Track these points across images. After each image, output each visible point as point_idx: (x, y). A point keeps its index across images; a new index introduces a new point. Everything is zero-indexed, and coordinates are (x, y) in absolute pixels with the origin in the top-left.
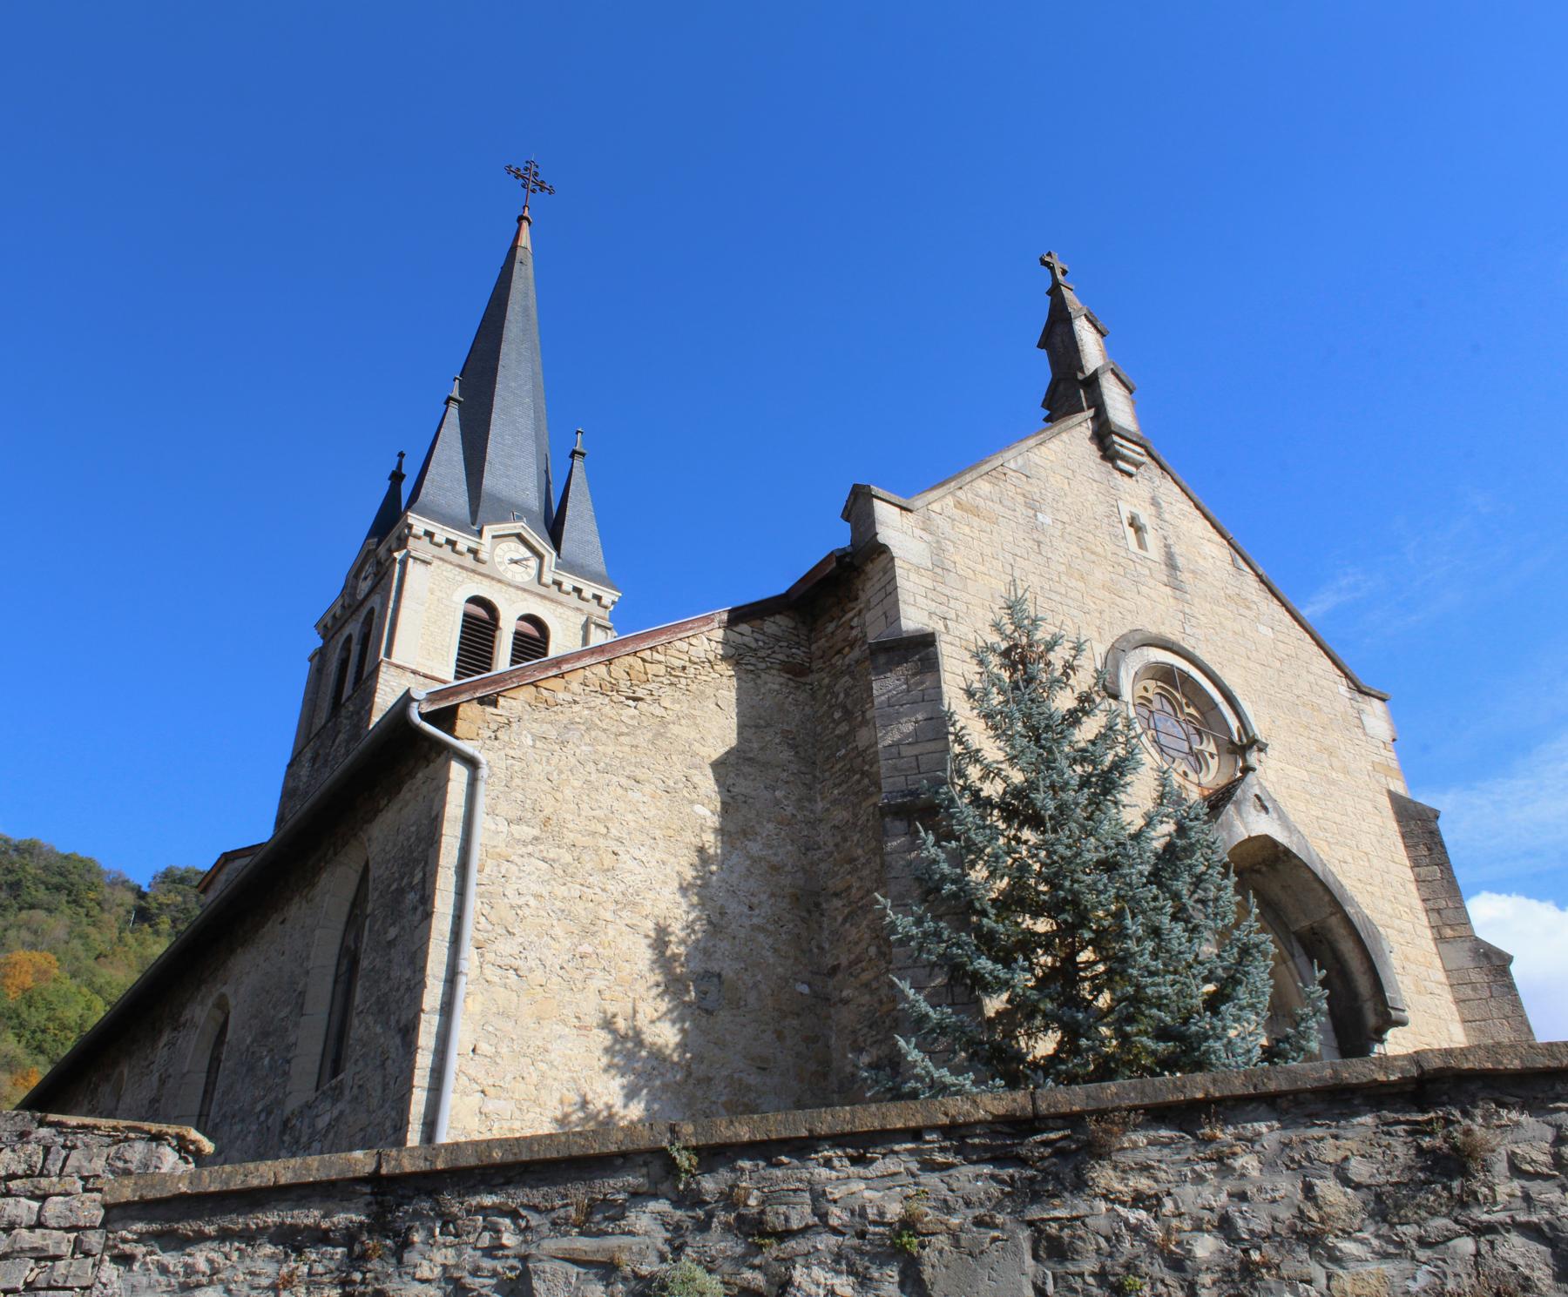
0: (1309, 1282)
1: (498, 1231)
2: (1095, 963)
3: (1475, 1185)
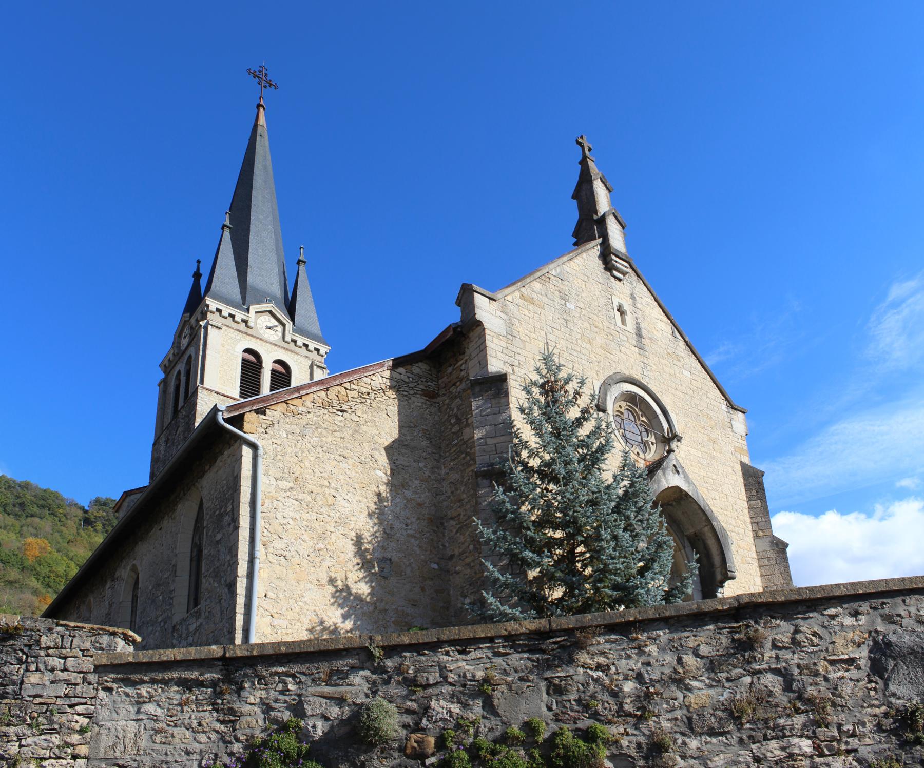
0: (675, 699)
1: (286, 683)
2: (584, 553)
3: (756, 654)
